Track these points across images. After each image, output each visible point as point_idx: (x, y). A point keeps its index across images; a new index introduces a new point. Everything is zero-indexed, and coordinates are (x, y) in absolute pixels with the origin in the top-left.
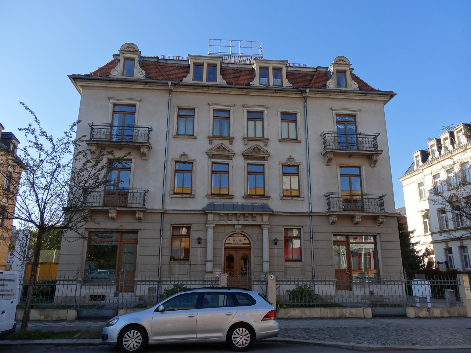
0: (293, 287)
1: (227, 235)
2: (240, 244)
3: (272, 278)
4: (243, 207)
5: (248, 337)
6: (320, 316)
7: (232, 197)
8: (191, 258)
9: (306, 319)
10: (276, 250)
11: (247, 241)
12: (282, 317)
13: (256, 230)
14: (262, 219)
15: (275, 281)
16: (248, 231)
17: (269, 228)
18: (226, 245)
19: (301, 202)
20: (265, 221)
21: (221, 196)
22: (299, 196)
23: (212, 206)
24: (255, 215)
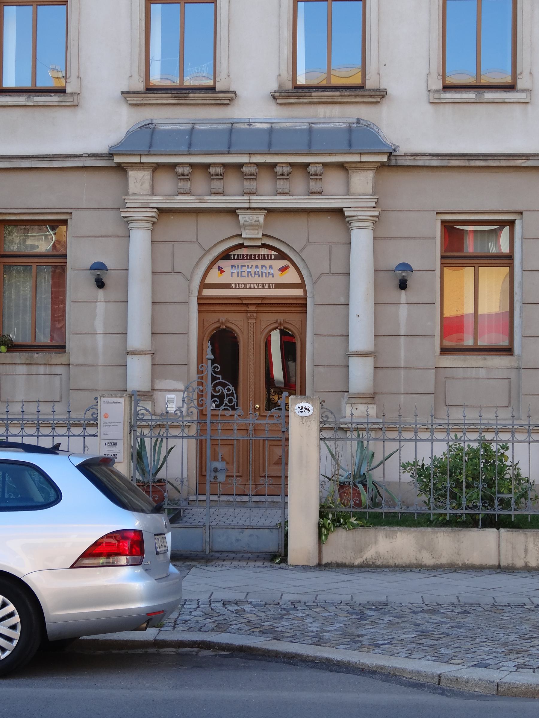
0: (440, 450)
1: (207, 252)
2: (262, 286)
3: (306, 413)
4: (271, 137)
5: (13, 627)
6: (493, 562)
7: (229, 98)
8: (72, 343)
9: (436, 568)
10: (403, 311)
11: (291, 277)
12: (340, 560)
13: (326, 229)
14: (348, 184)
15: (315, 426)
16: (290, 233)
17: (376, 221)
18: (207, 292)
19: (518, 108)
20: (358, 192)
21: (180, 93)
22: (511, 87)
23: (147, 136)
24: (319, 169)
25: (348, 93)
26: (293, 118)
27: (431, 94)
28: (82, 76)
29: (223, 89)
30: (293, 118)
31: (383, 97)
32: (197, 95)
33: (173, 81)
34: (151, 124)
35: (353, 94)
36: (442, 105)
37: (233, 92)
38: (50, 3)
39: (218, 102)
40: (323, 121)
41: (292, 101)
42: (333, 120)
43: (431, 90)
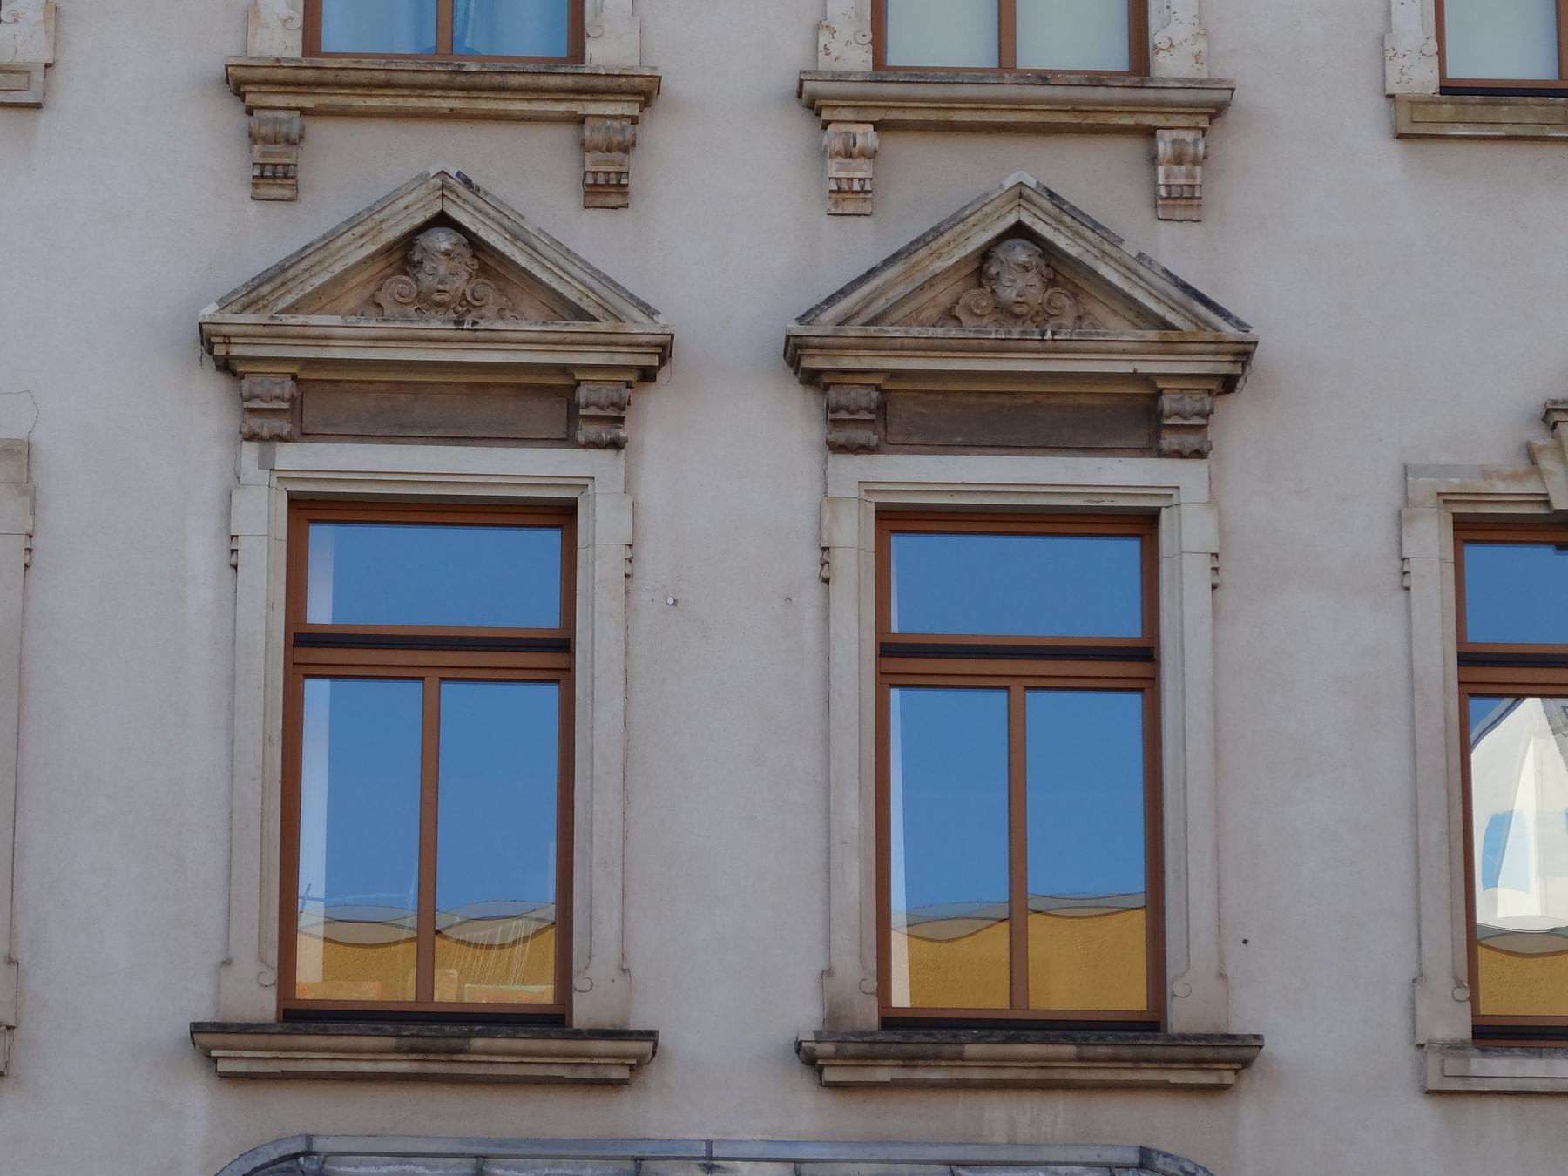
7: (629, 1055)
25: (1109, 1050)
26: (881, 1143)
27: (1433, 1060)
28: (23, 956)
29: (604, 1020)
30: (881, 1143)
31: (1246, 1063)
32: (501, 1043)
33: (383, 983)
34: (308, 1154)
35: (1127, 1052)
36: (1472, 1104)
37: (650, 1035)
38: (497, 674)
39: (587, 1073)
40: (1004, 1155)
41: (883, 1074)
42: (1044, 1155)
43: (1431, 1042)
